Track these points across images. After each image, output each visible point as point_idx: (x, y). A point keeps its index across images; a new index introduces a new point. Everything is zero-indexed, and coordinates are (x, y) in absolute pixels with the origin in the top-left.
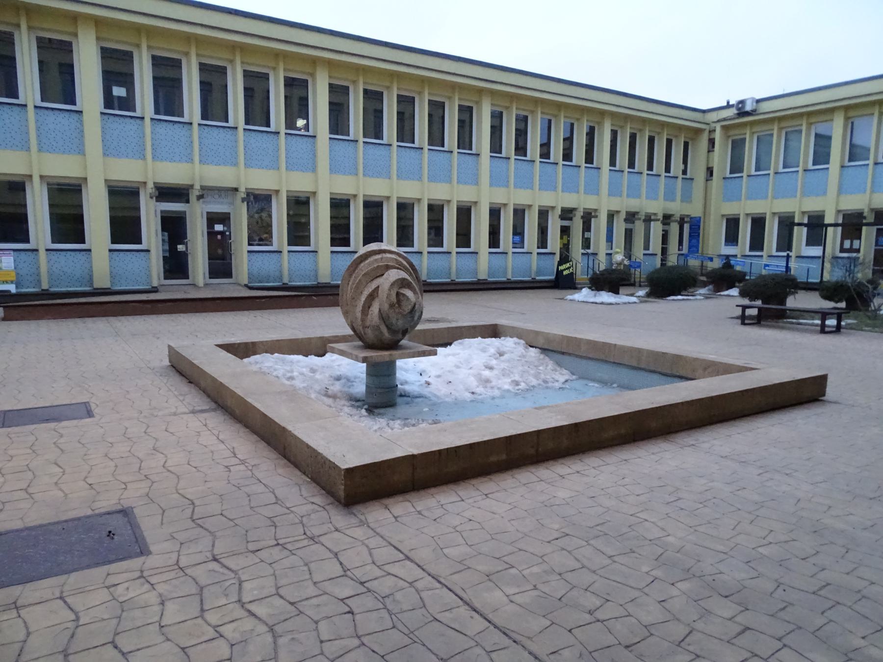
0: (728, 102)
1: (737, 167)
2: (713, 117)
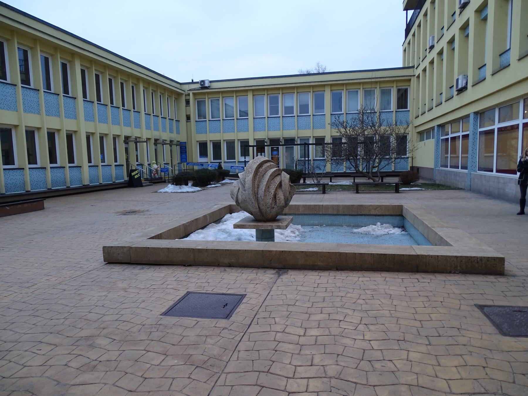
0: (193, 81)
1: (201, 115)
2: (186, 87)
